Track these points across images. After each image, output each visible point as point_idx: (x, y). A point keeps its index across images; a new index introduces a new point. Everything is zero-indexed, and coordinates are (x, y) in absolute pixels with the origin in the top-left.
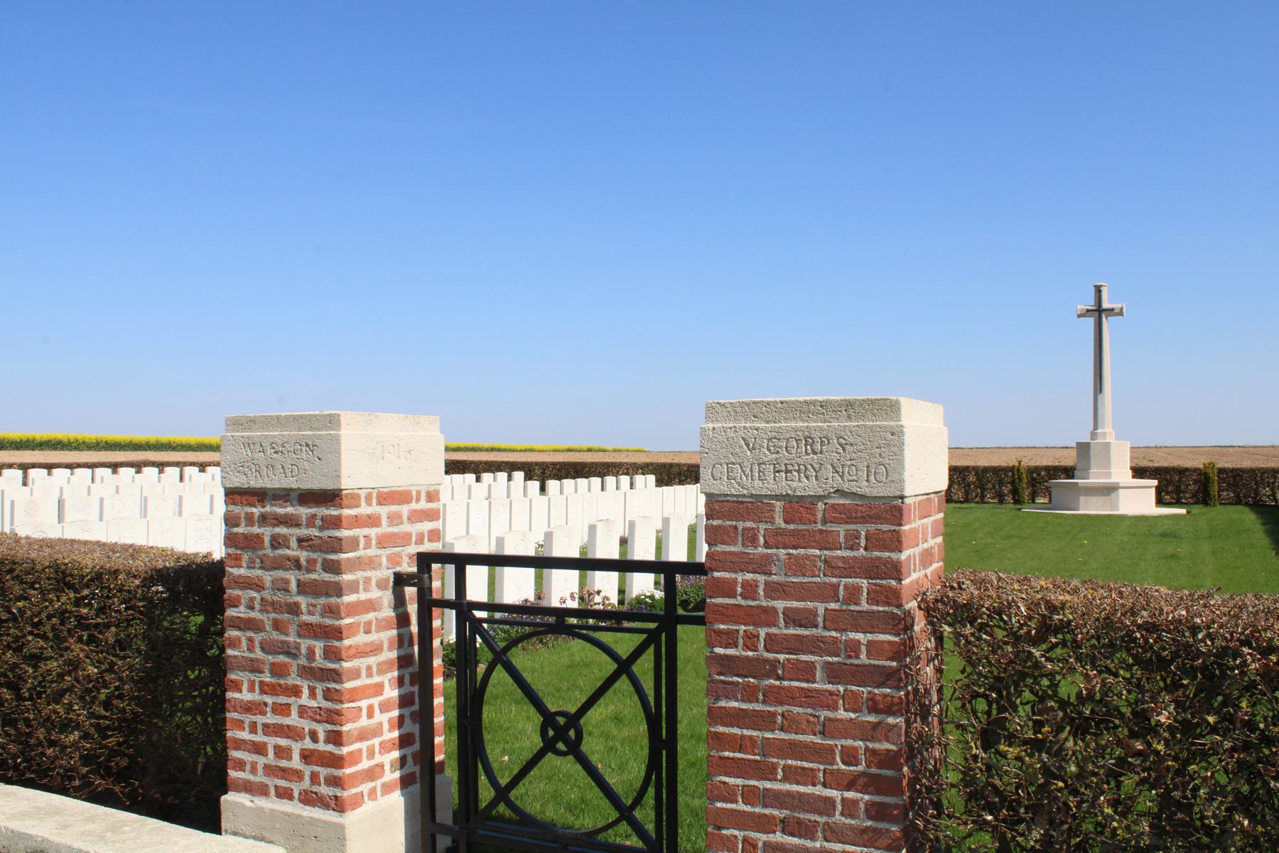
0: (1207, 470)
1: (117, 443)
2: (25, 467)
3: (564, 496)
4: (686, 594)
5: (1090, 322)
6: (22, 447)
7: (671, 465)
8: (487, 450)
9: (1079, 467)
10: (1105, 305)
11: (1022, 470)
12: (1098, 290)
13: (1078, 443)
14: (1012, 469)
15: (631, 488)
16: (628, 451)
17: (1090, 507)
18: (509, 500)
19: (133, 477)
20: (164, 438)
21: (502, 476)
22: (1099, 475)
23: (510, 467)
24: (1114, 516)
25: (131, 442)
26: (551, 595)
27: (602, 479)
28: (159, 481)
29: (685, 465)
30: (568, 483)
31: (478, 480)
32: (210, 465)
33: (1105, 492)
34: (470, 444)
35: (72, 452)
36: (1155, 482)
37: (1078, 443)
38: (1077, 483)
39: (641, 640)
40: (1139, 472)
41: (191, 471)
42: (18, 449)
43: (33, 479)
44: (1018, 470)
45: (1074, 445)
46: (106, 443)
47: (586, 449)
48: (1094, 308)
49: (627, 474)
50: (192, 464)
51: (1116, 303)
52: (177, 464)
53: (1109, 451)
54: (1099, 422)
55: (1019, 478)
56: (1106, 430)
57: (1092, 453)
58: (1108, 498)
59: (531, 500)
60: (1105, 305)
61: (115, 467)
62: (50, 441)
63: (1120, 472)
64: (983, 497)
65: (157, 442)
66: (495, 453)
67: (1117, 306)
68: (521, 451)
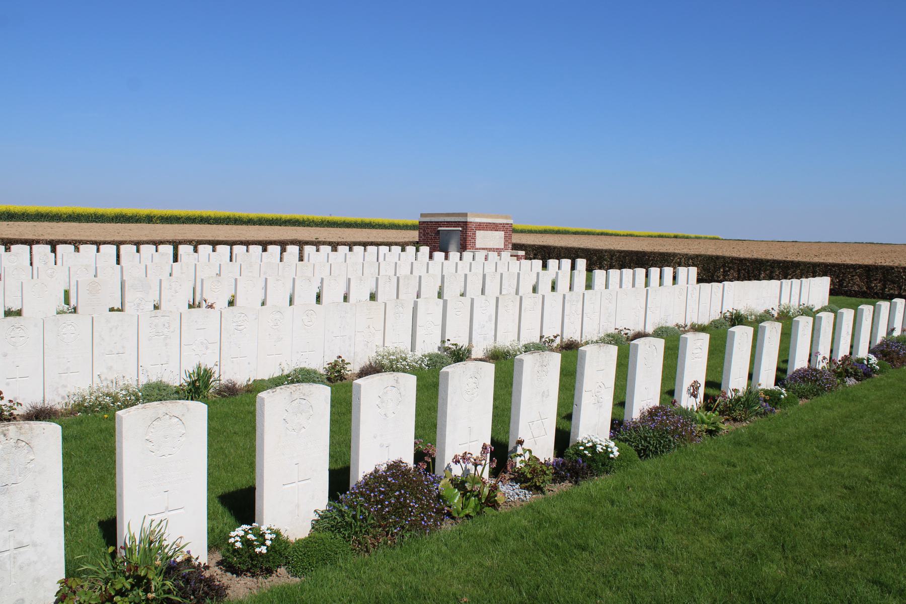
4: (645, 440)
6: (273, 223)
7: (718, 257)
19: (400, 254)
20: (367, 219)
21: (566, 263)
25: (344, 222)
26: (444, 450)
29: (729, 258)
30: (614, 273)
31: (545, 266)
32: (124, 244)
34: (358, 219)
35: (305, 228)
41: (127, 250)
42: (271, 225)
43: (181, 254)
46: (328, 222)
52: (301, 244)
65: (362, 221)
68: (624, 235)
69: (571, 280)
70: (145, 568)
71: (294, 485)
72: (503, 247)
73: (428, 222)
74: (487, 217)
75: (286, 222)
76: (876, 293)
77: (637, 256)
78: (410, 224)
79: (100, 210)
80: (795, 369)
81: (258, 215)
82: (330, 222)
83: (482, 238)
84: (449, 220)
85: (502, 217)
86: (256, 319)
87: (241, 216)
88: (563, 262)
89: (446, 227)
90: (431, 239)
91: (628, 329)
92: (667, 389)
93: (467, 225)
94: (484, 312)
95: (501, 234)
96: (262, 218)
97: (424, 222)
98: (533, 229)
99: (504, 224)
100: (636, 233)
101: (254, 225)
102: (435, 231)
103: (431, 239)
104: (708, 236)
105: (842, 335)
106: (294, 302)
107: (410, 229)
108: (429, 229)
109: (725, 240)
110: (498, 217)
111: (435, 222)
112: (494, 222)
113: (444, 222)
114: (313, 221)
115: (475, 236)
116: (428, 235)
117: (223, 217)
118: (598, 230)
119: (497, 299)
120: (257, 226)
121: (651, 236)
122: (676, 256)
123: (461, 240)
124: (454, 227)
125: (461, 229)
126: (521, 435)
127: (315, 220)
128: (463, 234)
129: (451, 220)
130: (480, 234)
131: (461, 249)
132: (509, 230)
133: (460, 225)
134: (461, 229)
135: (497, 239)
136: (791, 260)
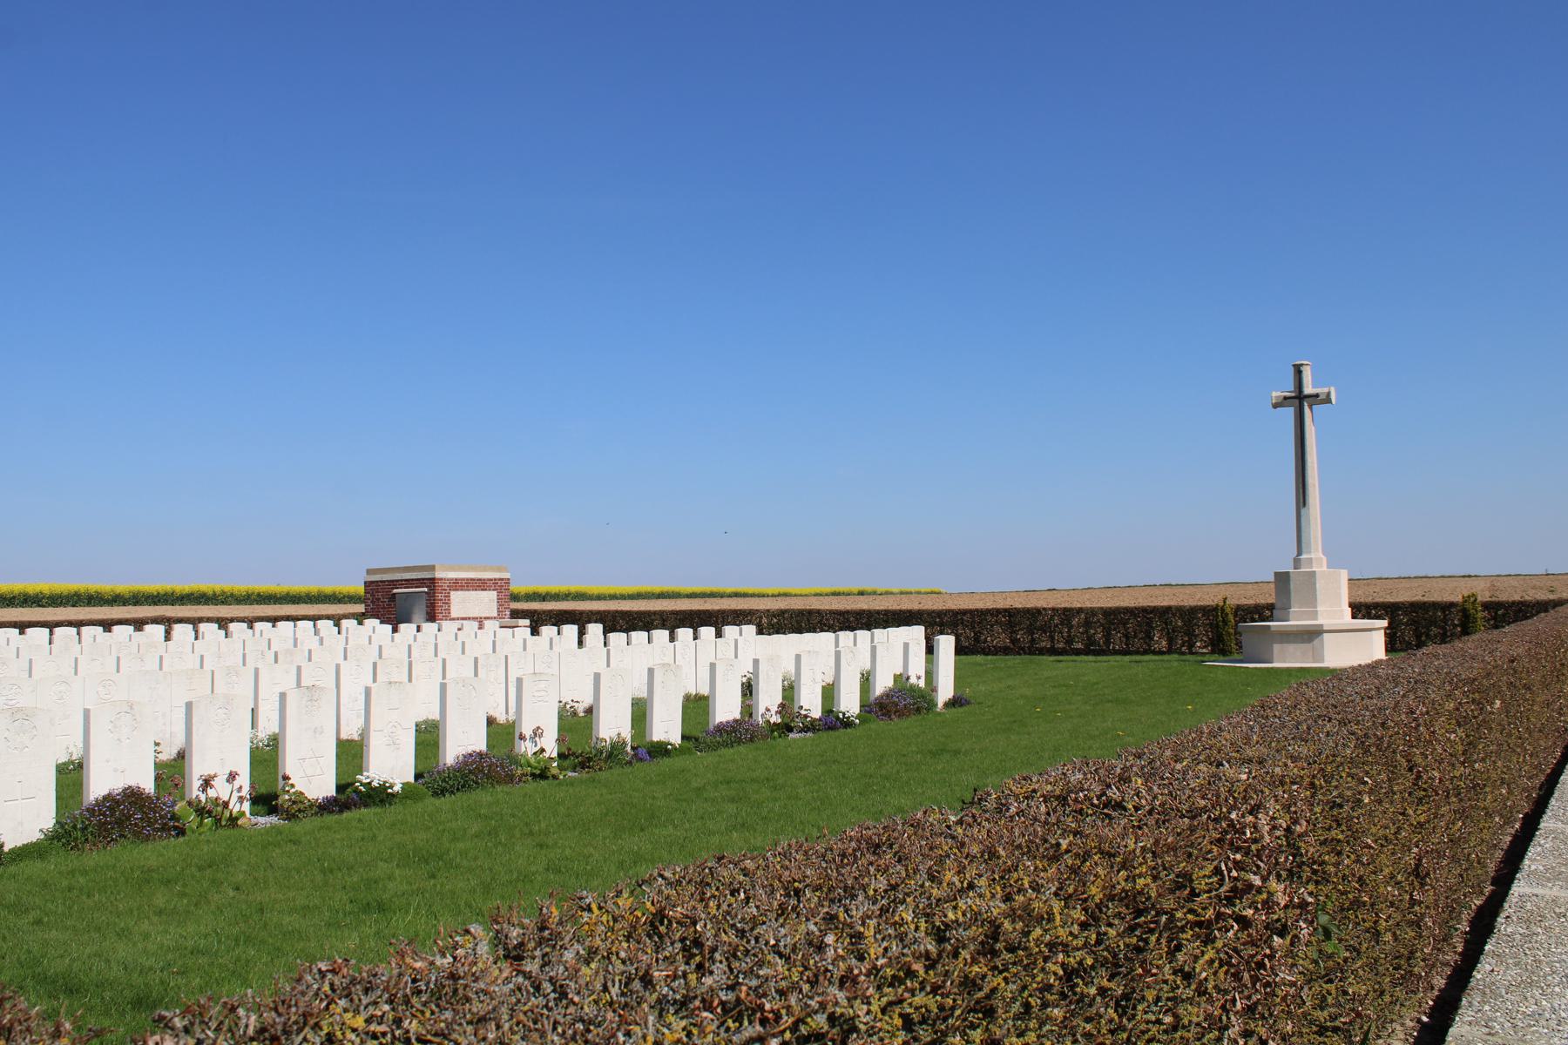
0: (1468, 606)
2: (169, 623)
5: (1289, 412)
6: (159, 601)
8: (730, 596)
9: (1278, 606)
10: (1308, 389)
11: (1228, 610)
12: (1298, 371)
14: (1215, 609)
15: (226, 637)
16: (919, 593)
17: (1287, 658)
18: (441, 655)
20: (328, 589)
22: (1301, 616)
23: (581, 620)
24: (1320, 668)
25: (288, 594)
27: (51, 633)
28: (393, 640)
32: (148, 623)
33: (1306, 637)
34: (312, 587)
36: (1384, 623)
37: (1276, 574)
38: (1269, 626)
40: (1360, 610)
43: (203, 633)
44: (1223, 609)
45: (1272, 579)
46: (259, 595)
47: (856, 591)
48: (1293, 394)
49: (663, 627)
50: (209, 620)
51: (1321, 387)
53: (1315, 584)
54: (1304, 545)
55: (1224, 621)
56: (1313, 556)
57: (1292, 586)
58: (1311, 645)
60: (1308, 389)
61: (107, 625)
62: (192, 594)
63: (1333, 609)
64: (1191, 645)
66: (740, 600)
67: (1322, 390)
68: (773, 596)
72: (496, 615)
73: (377, 582)
74: (467, 570)
75: (183, 598)
76: (1023, 649)
77: (699, 618)
80: (717, 722)
81: (132, 588)
82: (262, 596)
83: (461, 602)
84: (408, 577)
85: (492, 569)
86: (33, 691)
87: (99, 591)
88: (564, 630)
90: (384, 608)
91: (577, 702)
93: (435, 583)
94: (356, 681)
95: (493, 595)
96: (139, 592)
97: (372, 582)
99: (495, 580)
101: (124, 605)
104: (923, 590)
105: (802, 683)
110: (485, 570)
111: (388, 581)
112: (480, 577)
113: (402, 580)
114: (232, 595)
115: (449, 600)
117: (65, 593)
118: (729, 590)
119: (375, 665)
120: (130, 607)
121: (820, 595)
122: (754, 614)
123: (427, 607)
124: (416, 587)
125: (426, 590)
126: (288, 773)
127: (235, 592)
129: (412, 577)
130: (456, 596)
132: (499, 585)
134: (426, 590)
135: (486, 602)
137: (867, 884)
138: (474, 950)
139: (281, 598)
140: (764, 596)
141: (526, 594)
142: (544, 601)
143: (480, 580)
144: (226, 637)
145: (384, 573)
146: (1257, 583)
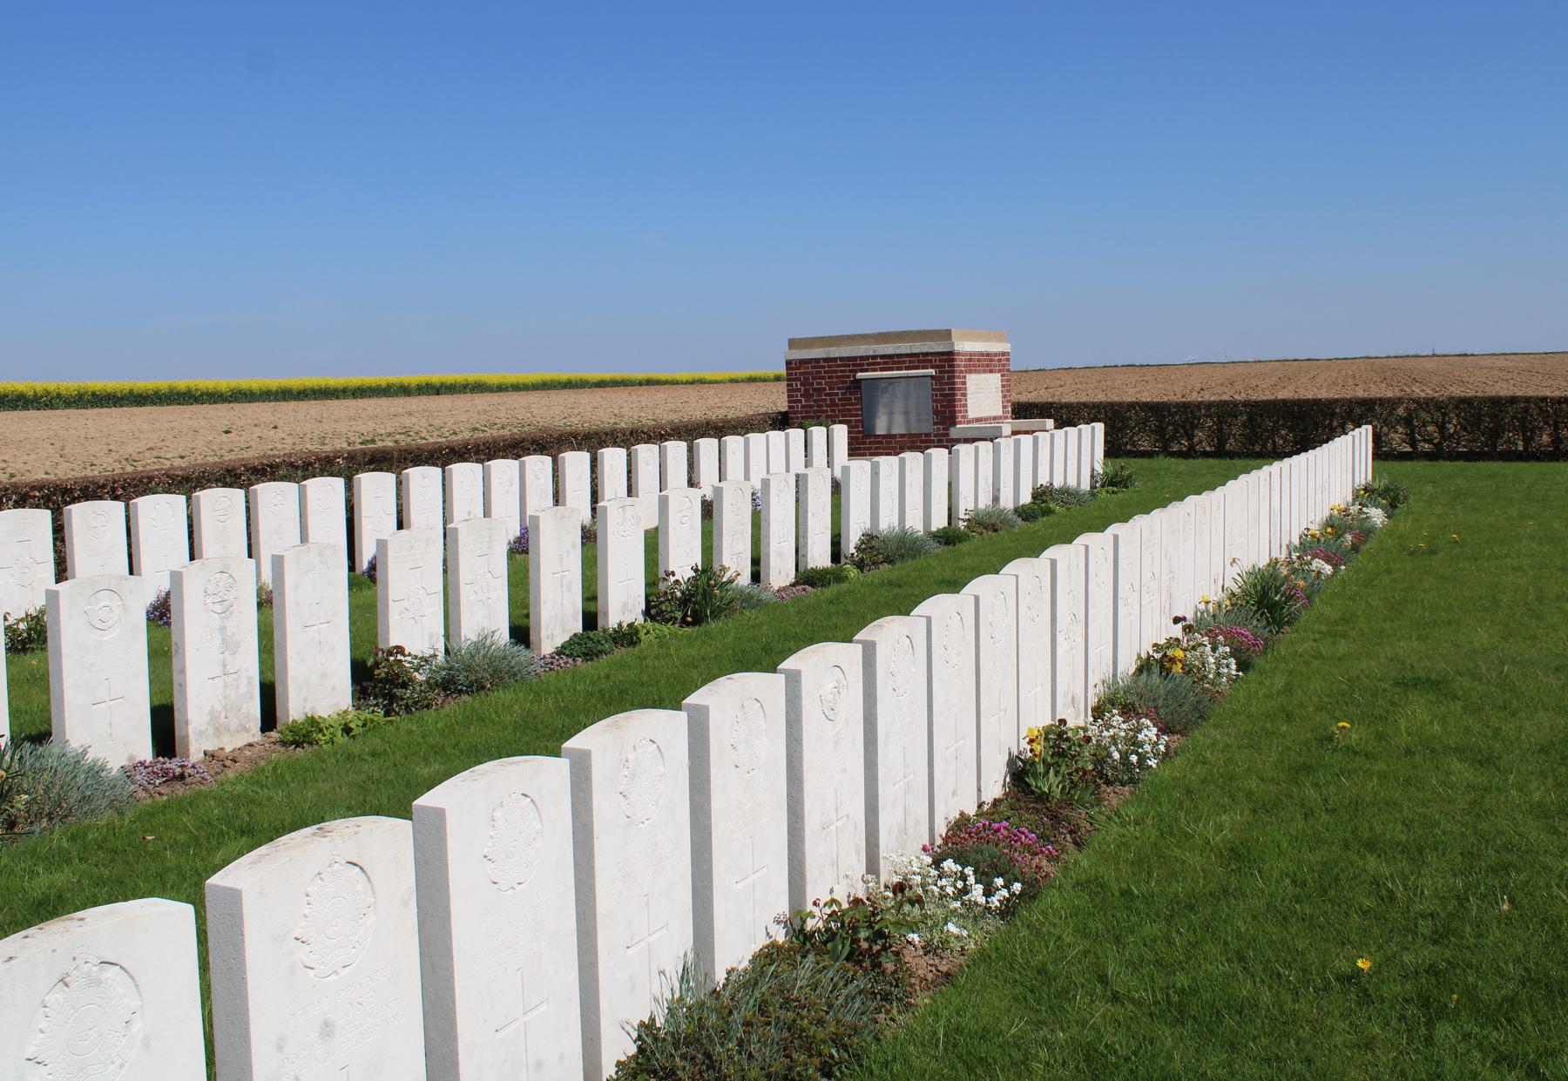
1: (109, 395)
3: (793, 472)
13: (312, 716)
15: (629, 496)
18: (707, 487)
20: (182, 384)
25: (131, 392)
34: (162, 383)
39: (568, 742)
46: (94, 394)
47: (772, 377)
59: (788, 470)
68: (687, 383)
69: (629, 478)
70: (1284, 851)
71: (103, 705)
72: (1001, 414)
73: (817, 360)
78: (274, 389)
79: (53, 385)
89: (882, 370)
92: (589, 595)
98: (520, 381)
100: (708, 376)
102: (843, 382)
103: (833, 404)
106: (201, 549)
107: (276, 400)
108: (823, 378)
109: (1396, 357)
111: (842, 359)
113: (874, 357)
114: (59, 395)
116: (820, 395)
123: (934, 401)
125: (932, 371)
128: (942, 384)
129: (898, 352)
131: (935, 424)
133: (930, 361)
134: (932, 371)
136: (1283, 397)
137: (1137, 696)
138: (1116, 998)
139: (122, 398)
140: (677, 383)
141: (427, 384)
142: (438, 394)
143: (988, 355)
144: (629, 496)
145: (831, 345)
146: (1233, 362)
